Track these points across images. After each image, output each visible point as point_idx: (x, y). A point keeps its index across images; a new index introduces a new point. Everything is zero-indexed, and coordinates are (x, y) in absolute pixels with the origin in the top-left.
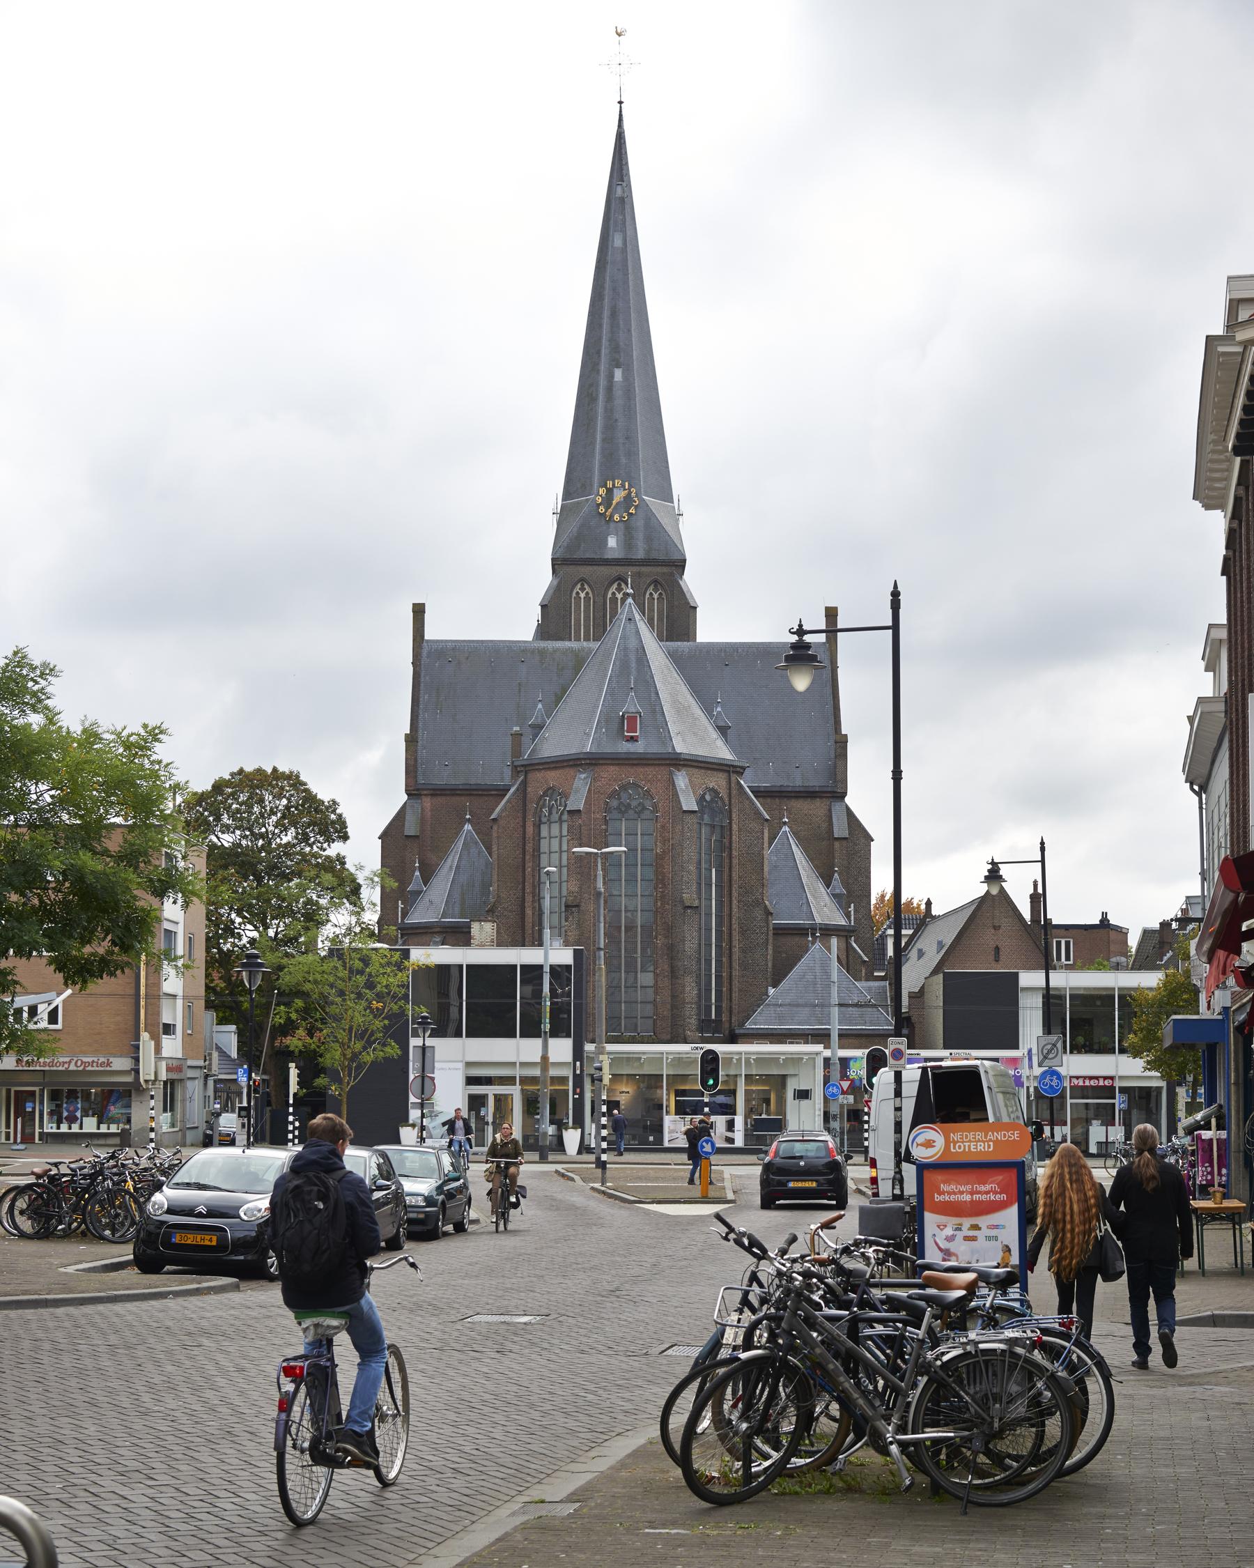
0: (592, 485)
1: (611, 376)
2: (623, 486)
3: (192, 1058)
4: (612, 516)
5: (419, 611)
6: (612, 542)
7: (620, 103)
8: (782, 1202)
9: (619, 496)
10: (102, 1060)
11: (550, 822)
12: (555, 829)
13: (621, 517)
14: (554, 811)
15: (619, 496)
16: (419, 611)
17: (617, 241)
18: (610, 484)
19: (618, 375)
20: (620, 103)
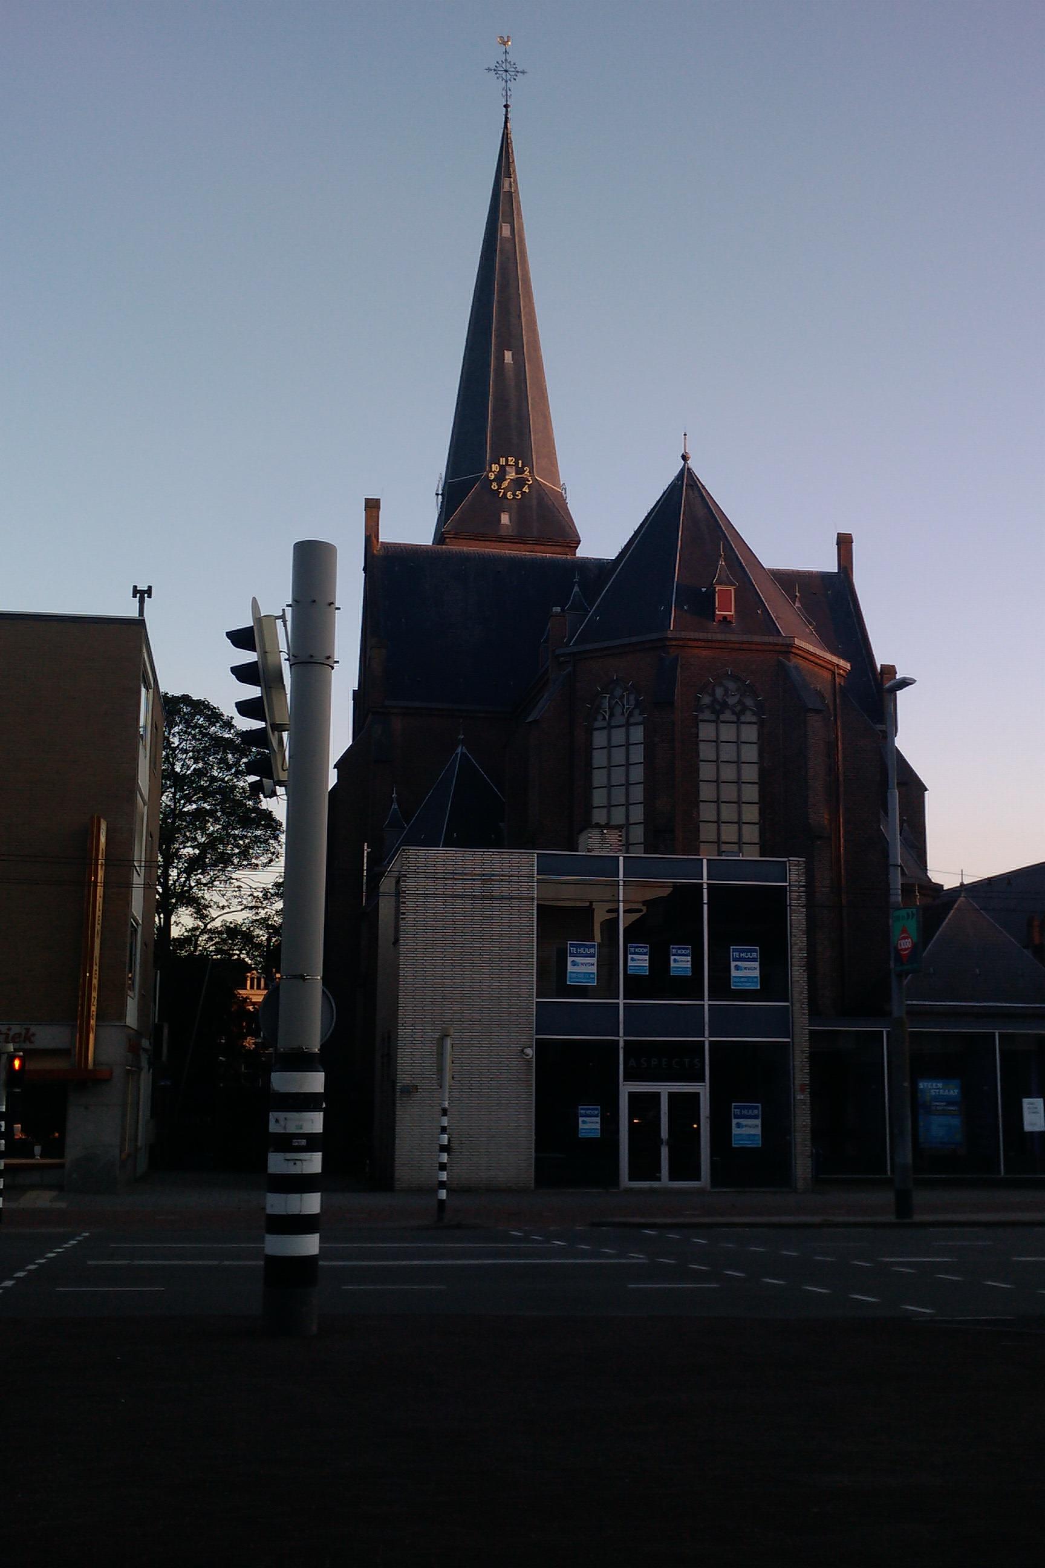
0: (484, 462)
1: (501, 358)
2: (517, 463)
3: (122, 1015)
4: (505, 494)
5: (372, 507)
6: (505, 519)
7: (506, 106)
8: (166, 1031)
9: (512, 475)
10: (16, 1029)
11: (610, 727)
12: (619, 736)
13: (514, 495)
14: (618, 710)
15: (512, 475)
16: (372, 507)
17: (506, 231)
18: (503, 461)
19: (508, 356)
20: (506, 106)
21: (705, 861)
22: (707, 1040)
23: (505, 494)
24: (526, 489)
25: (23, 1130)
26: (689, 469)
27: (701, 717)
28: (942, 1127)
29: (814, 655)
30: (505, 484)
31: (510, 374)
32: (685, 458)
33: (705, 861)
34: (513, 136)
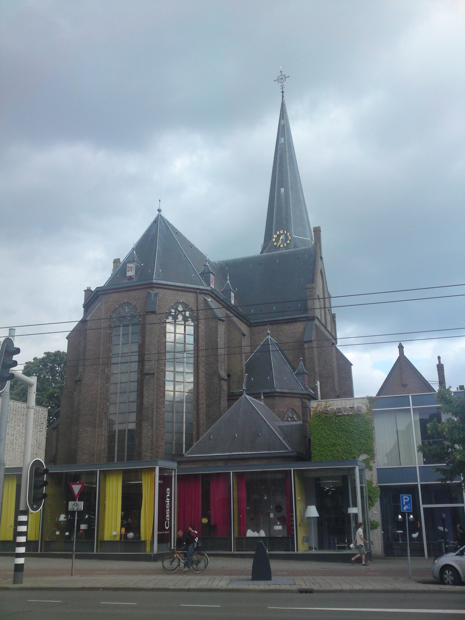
1: (279, 191)
4: (280, 246)
7: (283, 92)
18: (278, 233)
19: (282, 190)
20: (283, 92)
21: (410, 397)
22: (419, 483)
23: (280, 246)
24: (288, 242)
25: (415, 533)
26: (161, 215)
27: (167, 321)
28: (81, 505)
29: (175, 286)
30: (280, 241)
31: (283, 197)
32: (159, 211)
33: (410, 397)
34: (286, 103)
